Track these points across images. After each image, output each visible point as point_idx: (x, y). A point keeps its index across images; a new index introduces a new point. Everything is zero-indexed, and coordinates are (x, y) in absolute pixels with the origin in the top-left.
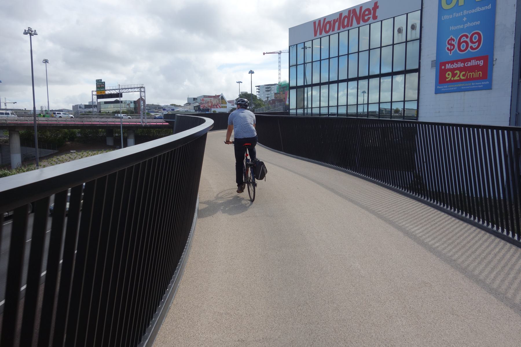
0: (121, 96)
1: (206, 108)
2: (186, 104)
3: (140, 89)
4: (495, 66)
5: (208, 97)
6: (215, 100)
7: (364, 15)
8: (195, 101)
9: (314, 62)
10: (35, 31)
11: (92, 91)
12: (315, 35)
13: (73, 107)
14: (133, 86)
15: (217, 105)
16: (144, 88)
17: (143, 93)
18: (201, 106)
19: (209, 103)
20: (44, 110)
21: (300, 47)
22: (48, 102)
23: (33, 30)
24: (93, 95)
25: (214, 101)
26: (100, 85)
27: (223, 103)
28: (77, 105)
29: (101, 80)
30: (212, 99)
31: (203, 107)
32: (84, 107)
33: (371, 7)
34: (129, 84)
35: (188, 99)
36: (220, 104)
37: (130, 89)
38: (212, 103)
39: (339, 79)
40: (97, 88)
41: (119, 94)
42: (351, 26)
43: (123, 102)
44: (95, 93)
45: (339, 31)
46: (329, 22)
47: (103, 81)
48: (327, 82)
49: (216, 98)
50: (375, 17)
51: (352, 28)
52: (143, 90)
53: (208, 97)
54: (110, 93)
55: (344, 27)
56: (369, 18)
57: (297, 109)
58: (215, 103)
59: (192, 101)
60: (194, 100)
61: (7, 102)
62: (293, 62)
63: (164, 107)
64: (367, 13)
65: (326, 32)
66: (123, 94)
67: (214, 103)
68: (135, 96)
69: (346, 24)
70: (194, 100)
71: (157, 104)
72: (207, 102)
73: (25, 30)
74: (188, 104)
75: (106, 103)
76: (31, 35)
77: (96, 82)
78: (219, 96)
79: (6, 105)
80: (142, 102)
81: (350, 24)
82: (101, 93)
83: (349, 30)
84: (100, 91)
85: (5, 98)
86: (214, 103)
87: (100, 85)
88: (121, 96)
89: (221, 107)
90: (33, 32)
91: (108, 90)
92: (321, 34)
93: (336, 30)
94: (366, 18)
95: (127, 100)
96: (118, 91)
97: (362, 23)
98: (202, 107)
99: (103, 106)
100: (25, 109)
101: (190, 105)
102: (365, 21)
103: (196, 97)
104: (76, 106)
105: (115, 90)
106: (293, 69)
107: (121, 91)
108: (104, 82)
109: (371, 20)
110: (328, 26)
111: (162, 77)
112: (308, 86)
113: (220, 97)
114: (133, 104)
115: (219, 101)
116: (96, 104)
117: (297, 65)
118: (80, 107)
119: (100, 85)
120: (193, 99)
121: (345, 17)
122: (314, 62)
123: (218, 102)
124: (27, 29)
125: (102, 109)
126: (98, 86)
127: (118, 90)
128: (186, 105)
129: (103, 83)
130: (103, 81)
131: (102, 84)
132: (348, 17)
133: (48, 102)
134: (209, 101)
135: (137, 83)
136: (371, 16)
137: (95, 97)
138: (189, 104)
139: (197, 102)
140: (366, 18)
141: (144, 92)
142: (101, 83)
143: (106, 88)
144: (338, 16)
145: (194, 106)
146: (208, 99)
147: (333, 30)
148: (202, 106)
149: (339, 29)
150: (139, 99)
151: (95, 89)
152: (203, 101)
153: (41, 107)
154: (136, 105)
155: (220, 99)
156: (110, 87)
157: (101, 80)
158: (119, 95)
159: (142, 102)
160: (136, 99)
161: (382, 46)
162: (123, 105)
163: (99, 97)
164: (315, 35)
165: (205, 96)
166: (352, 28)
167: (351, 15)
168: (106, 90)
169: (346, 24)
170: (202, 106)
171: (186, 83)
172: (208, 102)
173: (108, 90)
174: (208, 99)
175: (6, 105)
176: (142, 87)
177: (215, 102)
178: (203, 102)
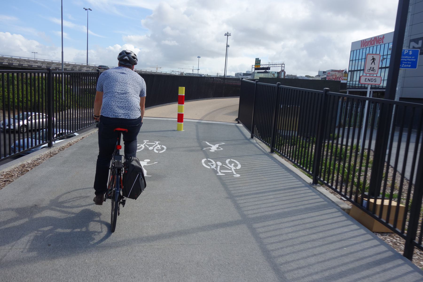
0: (270, 69)
1: (331, 79)
2: (317, 76)
3: (282, 65)
4: (293, 75)
5: (334, 71)
6: (339, 74)
7: (379, 41)
8: (324, 74)
9: (363, 59)
10: (230, 34)
11: (252, 65)
12: (361, 47)
13: (236, 74)
14: (277, 63)
15: (340, 78)
16: (284, 64)
17: (283, 68)
18: (327, 78)
19: (334, 76)
20: (219, 75)
21: (355, 52)
22: (62, 52)
23: (229, 33)
24: (252, 68)
25: (338, 74)
26: (258, 61)
27: (346, 76)
28: (239, 73)
29: (259, 59)
30: (337, 73)
31: (329, 79)
32: (242, 75)
33: (382, 37)
34: (275, 62)
35: (319, 72)
36: (342, 77)
37: (275, 65)
38: (336, 75)
39: (355, 70)
40: (256, 63)
41: (268, 67)
42: (374, 44)
43: (270, 73)
44: (254, 67)
45: (370, 46)
46: (367, 42)
47: (259, 59)
48: (387, 68)
49: (340, 72)
50: (383, 42)
51: (374, 45)
52: (283, 66)
53: (333, 71)
54: (263, 67)
55: (372, 45)
56: (381, 42)
57: (350, 81)
58: (338, 76)
59: (322, 74)
60: (323, 73)
61: (158, 67)
62: (351, 59)
63: (299, 77)
64: (380, 40)
65: (365, 46)
66: (271, 68)
67: (338, 76)
68: (279, 70)
69: (372, 43)
70: (323, 73)
71: (295, 75)
72: (332, 75)
73: (225, 34)
74: (318, 76)
75: (258, 72)
76: (228, 36)
77: (255, 60)
78: (343, 71)
79: (193, 71)
80: (283, 73)
81: (374, 44)
82: (258, 66)
83: (373, 47)
84: (257, 65)
85: (193, 66)
86: (337, 76)
87: (258, 61)
88: (270, 69)
89: (343, 79)
90: (229, 34)
91: (262, 65)
92: (363, 47)
93: (369, 46)
94: (380, 42)
95: (273, 71)
96: (268, 66)
97: (378, 44)
98: (328, 79)
99: (256, 75)
100: (207, 74)
101: (319, 77)
102: (379, 43)
103: (325, 71)
104: (238, 74)
105: (266, 65)
106: (351, 62)
107: (270, 66)
108: (260, 60)
109: (381, 43)
110: (366, 43)
111: (305, 52)
112: (356, 71)
113: (344, 72)
114: (277, 73)
115: (342, 74)
116: (251, 73)
117: (353, 60)
118: (240, 75)
119: (258, 61)
120: (323, 72)
121: (373, 40)
122: (363, 59)
123: (341, 75)
124: (226, 33)
125: (255, 77)
126: (256, 62)
127: (268, 65)
128: (317, 76)
129: (259, 61)
130: (259, 59)
131: (259, 61)
132: (373, 40)
133: (62, 52)
134: (334, 74)
135: (280, 61)
136: (381, 41)
137: (254, 69)
138: (319, 76)
139: (326, 75)
140: (380, 42)
141: (284, 67)
142: (258, 60)
143: (261, 64)
144: (370, 40)
145: (322, 77)
146: (334, 73)
147: (368, 46)
148: (328, 78)
149: (370, 45)
150: (237, 118)
151: (254, 64)
152: (329, 74)
153: (217, 73)
154: (278, 75)
155: (343, 73)
156: (264, 63)
157: (259, 59)
158: (268, 68)
159: (283, 73)
160: (279, 71)
161: (384, 55)
162: (270, 74)
163: (256, 69)
164: (361, 47)
165: (333, 71)
166: (374, 45)
167: (375, 40)
168: (261, 65)
169: (372, 43)
170: (328, 78)
171: (326, 58)
172: (333, 75)
173: (262, 65)
174: (334, 73)
175: (193, 71)
176: (283, 64)
177: (339, 75)
178: (329, 75)
